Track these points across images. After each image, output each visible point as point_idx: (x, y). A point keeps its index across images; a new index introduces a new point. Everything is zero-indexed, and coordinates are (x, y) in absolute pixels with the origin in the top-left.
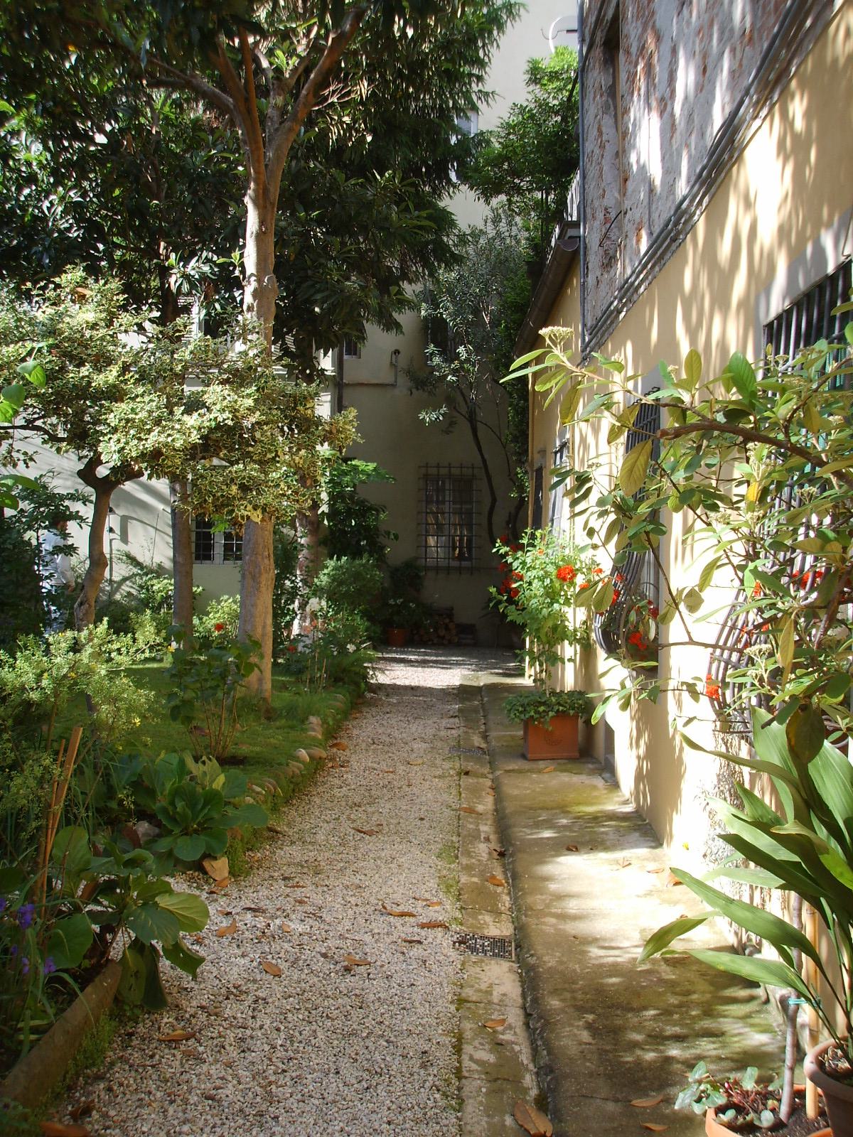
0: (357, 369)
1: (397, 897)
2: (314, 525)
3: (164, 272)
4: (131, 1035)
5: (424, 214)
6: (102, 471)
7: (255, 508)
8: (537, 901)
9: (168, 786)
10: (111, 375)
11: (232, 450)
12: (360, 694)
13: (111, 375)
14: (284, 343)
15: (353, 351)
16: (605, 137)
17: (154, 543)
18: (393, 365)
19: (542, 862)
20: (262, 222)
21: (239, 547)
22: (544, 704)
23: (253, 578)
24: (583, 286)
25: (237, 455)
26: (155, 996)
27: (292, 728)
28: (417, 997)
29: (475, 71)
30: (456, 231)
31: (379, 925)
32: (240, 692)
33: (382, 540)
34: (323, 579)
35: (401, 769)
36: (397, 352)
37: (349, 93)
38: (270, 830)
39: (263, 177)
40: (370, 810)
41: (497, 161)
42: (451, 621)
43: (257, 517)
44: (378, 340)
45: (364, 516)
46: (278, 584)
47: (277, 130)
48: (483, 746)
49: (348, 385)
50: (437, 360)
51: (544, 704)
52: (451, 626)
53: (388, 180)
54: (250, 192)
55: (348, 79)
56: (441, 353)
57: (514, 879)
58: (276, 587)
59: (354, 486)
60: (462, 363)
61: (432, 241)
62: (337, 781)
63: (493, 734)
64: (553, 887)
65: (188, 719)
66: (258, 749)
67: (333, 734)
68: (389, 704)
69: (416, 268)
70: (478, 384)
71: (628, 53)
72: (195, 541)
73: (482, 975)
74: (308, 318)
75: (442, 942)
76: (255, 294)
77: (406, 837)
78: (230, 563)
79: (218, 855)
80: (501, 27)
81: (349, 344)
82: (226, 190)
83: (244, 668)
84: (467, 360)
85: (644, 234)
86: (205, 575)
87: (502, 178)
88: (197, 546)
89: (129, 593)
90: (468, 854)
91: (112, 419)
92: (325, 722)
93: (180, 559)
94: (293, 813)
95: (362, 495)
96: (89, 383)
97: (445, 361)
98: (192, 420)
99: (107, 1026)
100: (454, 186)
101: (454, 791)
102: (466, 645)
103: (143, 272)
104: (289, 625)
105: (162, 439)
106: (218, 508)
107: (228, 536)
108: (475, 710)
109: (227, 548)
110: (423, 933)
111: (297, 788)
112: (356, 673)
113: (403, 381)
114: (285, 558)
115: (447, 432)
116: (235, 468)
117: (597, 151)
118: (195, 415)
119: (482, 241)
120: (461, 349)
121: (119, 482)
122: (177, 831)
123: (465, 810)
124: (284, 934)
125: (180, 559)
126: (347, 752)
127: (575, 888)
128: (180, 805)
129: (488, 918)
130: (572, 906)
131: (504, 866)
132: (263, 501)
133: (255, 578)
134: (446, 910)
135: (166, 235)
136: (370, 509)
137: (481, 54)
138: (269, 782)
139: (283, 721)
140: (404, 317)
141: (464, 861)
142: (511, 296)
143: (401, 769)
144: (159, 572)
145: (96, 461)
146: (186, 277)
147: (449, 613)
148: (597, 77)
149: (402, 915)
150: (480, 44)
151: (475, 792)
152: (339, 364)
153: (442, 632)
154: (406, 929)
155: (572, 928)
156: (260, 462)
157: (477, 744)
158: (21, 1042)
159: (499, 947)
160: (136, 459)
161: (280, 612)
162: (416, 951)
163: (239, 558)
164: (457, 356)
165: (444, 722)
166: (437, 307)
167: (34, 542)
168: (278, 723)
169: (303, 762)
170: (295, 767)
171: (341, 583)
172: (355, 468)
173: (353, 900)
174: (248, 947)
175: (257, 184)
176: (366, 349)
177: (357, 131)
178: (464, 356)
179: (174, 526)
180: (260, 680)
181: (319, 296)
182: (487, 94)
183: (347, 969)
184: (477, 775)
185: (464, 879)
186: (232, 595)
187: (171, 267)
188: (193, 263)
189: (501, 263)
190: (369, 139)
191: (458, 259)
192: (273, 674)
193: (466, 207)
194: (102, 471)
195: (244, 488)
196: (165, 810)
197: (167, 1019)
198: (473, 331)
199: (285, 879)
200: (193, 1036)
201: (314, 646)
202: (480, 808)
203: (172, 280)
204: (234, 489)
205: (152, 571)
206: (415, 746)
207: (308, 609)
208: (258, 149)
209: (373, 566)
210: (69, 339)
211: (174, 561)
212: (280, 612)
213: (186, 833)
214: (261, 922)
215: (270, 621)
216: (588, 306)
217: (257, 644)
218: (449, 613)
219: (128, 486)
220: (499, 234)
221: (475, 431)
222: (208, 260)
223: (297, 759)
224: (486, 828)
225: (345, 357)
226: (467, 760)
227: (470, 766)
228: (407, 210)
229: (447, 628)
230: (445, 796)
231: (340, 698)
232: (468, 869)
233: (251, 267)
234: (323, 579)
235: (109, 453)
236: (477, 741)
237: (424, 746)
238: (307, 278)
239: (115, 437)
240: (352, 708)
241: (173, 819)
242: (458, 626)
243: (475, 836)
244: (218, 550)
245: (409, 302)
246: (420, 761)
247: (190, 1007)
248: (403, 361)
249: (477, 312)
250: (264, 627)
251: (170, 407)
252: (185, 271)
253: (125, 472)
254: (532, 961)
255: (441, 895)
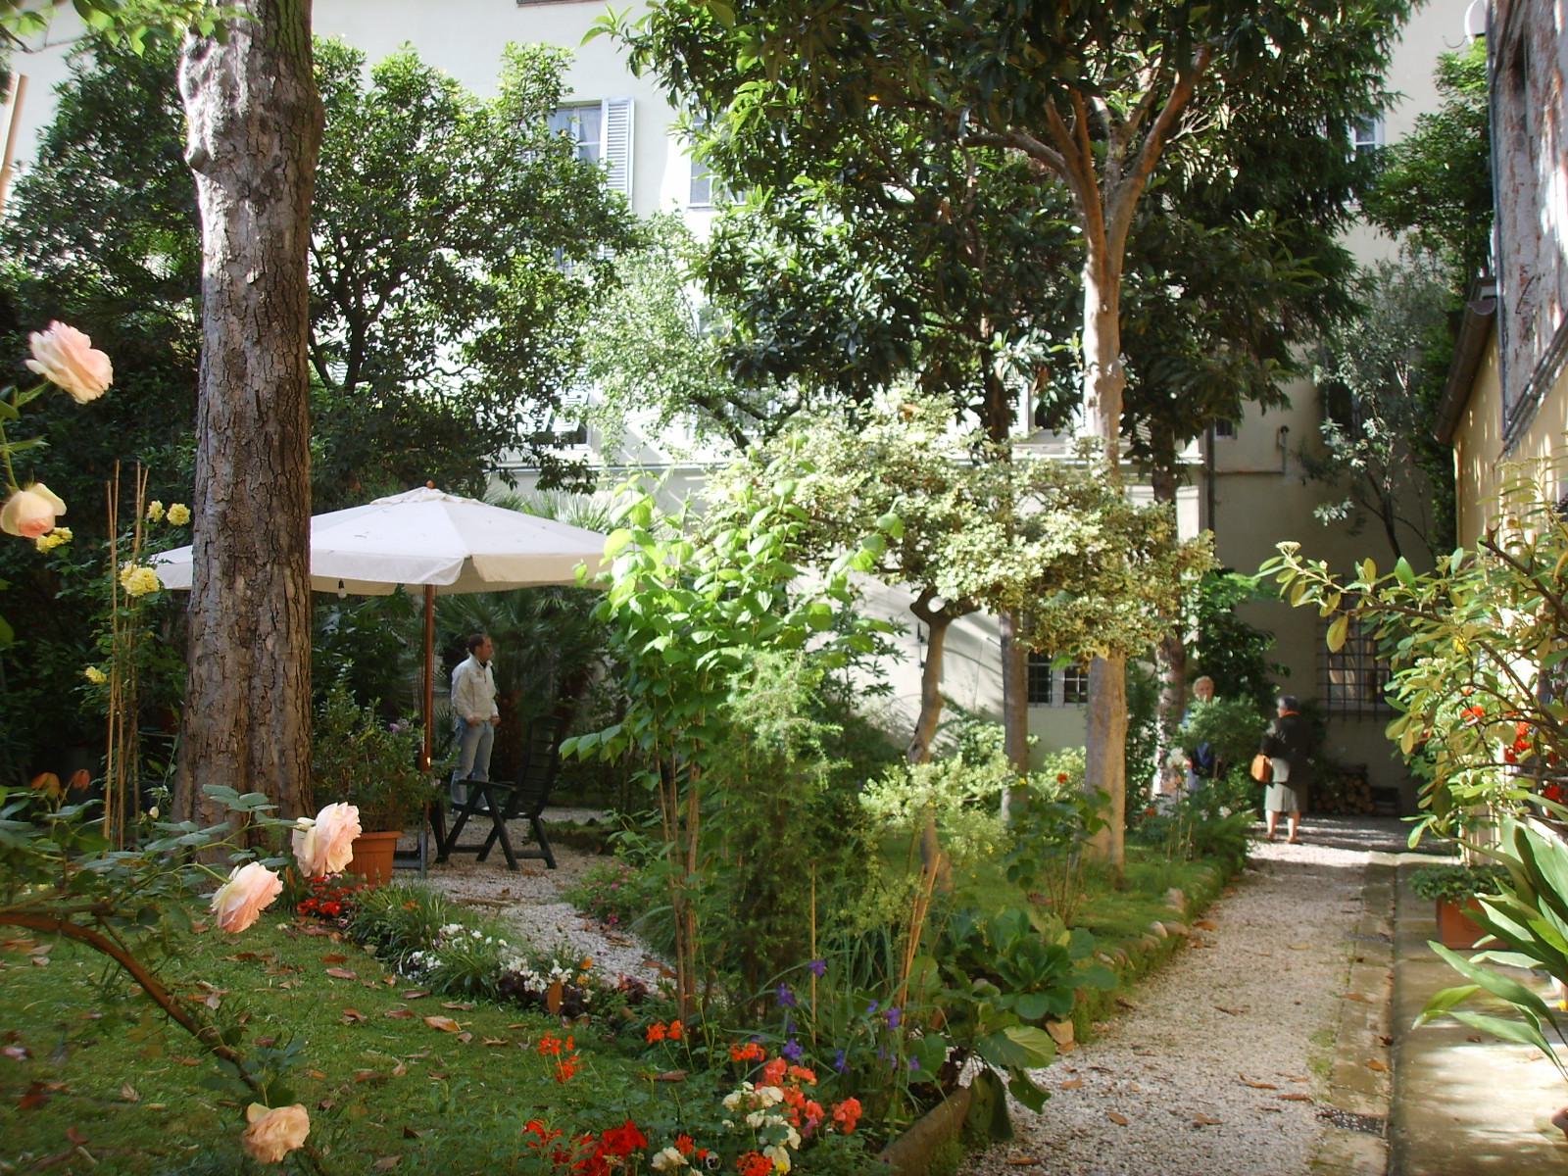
0: (1234, 453)
1: (1260, 1072)
2: (1177, 655)
3: (988, 356)
4: (979, 1158)
5: (1306, 261)
6: (935, 606)
7: (1102, 643)
8: (1420, 1086)
9: (1009, 943)
10: (946, 504)
11: (1075, 579)
12: (1228, 863)
13: (946, 504)
14: (1134, 434)
15: (1226, 429)
16: (1518, 180)
17: (976, 681)
18: (1280, 447)
19: (1429, 1051)
20: (1103, 300)
21: (1083, 687)
22: (1460, 879)
23: (1102, 723)
24: (1503, 357)
25: (1081, 585)
26: (1002, 1128)
27: (1147, 900)
28: (1269, 1156)
29: (1372, 72)
30: (1356, 276)
31: (1236, 1093)
32: (1087, 853)
33: (1269, 676)
34: (1189, 725)
35: (1279, 953)
36: (1284, 429)
37: (1205, 122)
38: (1120, 1003)
39: (1102, 247)
40: (1237, 991)
41: (1400, 187)
42: (1365, 782)
43: (1103, 653)
44: (1258, 421)
45: (1244, 644)
46: (1132, 730)
47: (1117, 188)
48: (1388, 932)
49: (1222, 475)
50: (1337, 439)
51: (1460, 879)
52: (1365, 789)
53: (1260, 222)
54: (1087, 266)
55: (1206, 105)
56: (1342, 430)
57: (1398, 1065)
58: (1129, 735)
59: (1232, 607)
60: (1370, 441)
61: (1323, 285)
62: (1200, 962)
63: (1401, 921)
64: (1442, 1074)
65: (1027, 882)
66: (1106, 921)
67: (1198, 912)
68: (1274, 883)
69: (1303, 323)
70: (1394, 469)
71: (1534, 85)
72: (1030, 680)
73: (1345, 1146)
74: (1164, 402)
75: (1306, 1114)
76: (1099, 386)
77: (1276, 1019)
78: (1073, 706)
79: (1062, 1016)
80: (1403, 18)
81: (1226, 421)
82: (1058, 254)
83: (1091, 824)
84: (1378, 438)
85: (1556, 307)
86: (1049, 719)
87: (1411, 206)
88: (1031, 685)
89: (946, 745)
90: (1348, 1039)
91: (950, 552)
92: (1187, 896)
93: (1011, 701)
94: (1147, 988)
95: (1242, 618)
96: (924, 515)
97: (1348, 439)
98: (1034, 551)
99: (955, 1146)
100: (1350, 218)
101: (1341, 978)
102: (1385, 816)
103: (965, 353)
104: (1148, 783)
105: (1003, 571)
106: (1062, 644)
107: (1069, 673)
108: (1385, 894)
109: (1069, 687)
110: (1284, 1104)
111: (1153, 962)
112: (1232, 844)
113: (1294, 468)
114: (1141, 702)
115: (1352, 533)
116: (1079, 601)
117: (1511, 195)
118: (1037, 545)
119: (1396, 280)
120: (1369, 424)
121: (955, 616)
122: (1018, 988)
123: (1352, 998)
124: (1131, 1092)
125: (1011, 701)
126: (1215, 933)
127: (1468, 1076)
128: (1022, 961)
129: (1360, 1098)
130: (1460, 1093)
131: (1389, 1054)
132: (1109, 636)
133: (1103, 723)
134: (1315, 1085)
135: (989, 310)
136: (1253, 635)
137: (1378, 49)
138: (1119, 951)
139: (1137, 893)
140: (1293, 388)
141: (1342, 1046)
142: (1434, 353)
143: (1279, 953)
144: (983, 717)
145: (930, 592)
146: (1014, 361)
147: (1362, 773)
148: (1506, 104)
149: (1261, 1087)
150: (1376, 37)
151: (1369, 981)
152: (1209, 450)
153: (1352, 799)
154: (1259, 1098)
155: (1452, 1111)
156: (1106, 594)
157: (1379, 930)
158: (887, 1135)
159: (1369, 1125)
160: (975, 595)
161: (1134, 765)
162: (1274, 1118)
163: (1083, 700)
164: (1364, 433)
165: (1342, 905)
166: (1335, 369)
167: (844, 681)
168: (1131, 895)
169: (1160, 936)
170: (1149, 940)
171: (1212, 731)
172: (1232, 583)
173: (1208, 1071)
174: (1094, 1100)
175: (1095, 255)
176: (1244, 429)
177: (1219, 165)
178: (1373, 432)
179: (1004, 663)
180: (1110, 844)
181: (1178, 377)
182: (1390, 96)
183: (1197, 1126)
184: (1372, 963)
185: (1338, 1061)
186: (1075, 747)
187: (996, 350)
188: (1023, 342)
189: (1419, 306)
190: (1234, 173)
191: (1356, 310)
192: (1126, 842)
193: (1366, 244)
194: (935, 606)
195: (1090, 622)
196: (1005, 967)
197: (1013, 1149)
198: (1386, 401)
199: (1135, 1048)
200: (1038, 1162)
201: (1178, 808)
202: (1371, 997)
203: (998, 365)
204: (1079, 624)
205: (973, 717)
206: (1300, 930)
207: (1169, 761)
208: (1095, 215)
209: (1254, 709)
210: (899, 463)
211: (1005, 705)
212: (1134, 765)
213: (1028, 990)
214: (1107, 1080)
215: (1121, 773)
216: (1509, 383)
217: (1105, 797)
218: (1362, 773)
219: (961, 624)
220: (1419, 268)
221: (1390, 531)
222: (1040, 340)
223: (1153, 932)
224: (1373, 1017)
225: (1217, 438)
226: (1364, 946)
227: (1366, 953)
228: (1284, 258)
229: (1358, 793)
230: (1330, 983)
231: (1207, 873)
232: (1345, 1053)
233: (1091, 356)
234: (1189, 725)
235: (947, 586)
236: (1381, 927)
237: (1311, 930)
238: (1160, 356)
239: (954, 571)
240: (1225, 885)
241: (1014, 976)
242: (1373, 789)
243: (1360, 1023)
244: (1057, 691)
245: (1297, 366)
246: (1303, 945)
247: (1035, 1142)
248: (1292, 441)
249: (1389, 374)
250: (1115, 781)
251: (1009, 535)
252: (1012, 356)
253: (964, 606)
254: (1402, 1136)
255: (1309, 1073)
